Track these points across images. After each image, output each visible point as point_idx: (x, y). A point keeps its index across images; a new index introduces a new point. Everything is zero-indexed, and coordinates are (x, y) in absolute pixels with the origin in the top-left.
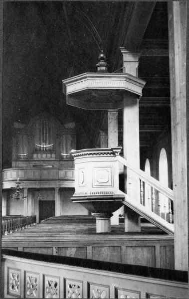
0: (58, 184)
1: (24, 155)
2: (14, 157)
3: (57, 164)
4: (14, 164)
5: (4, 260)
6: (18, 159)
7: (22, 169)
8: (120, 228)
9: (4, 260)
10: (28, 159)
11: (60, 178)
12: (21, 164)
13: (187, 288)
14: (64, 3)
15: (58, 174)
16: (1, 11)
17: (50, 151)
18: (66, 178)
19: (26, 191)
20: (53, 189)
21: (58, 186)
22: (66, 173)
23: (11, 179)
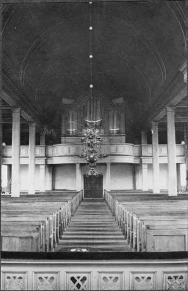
0: (110, 158)
1: (72, 130)
2: (63, 132)
3: (105, 140)
4: (63, 140)
5: (83, 290)
6: (67, 135)
7: (73, 144)
8: (9, 196)
9: (83, 290)
10: (77, 135)
11: (111, 153)
12: (68, 139)
13: (4, 208)
14: (22, 122)
15: (109, 149)
16: (1, 131)
17: (98, 126)
18: (118, 153)
19: (78, 166)
20: (105, 164)
21: (109, 161)
22: (117, 149)
23: (62, 155)
